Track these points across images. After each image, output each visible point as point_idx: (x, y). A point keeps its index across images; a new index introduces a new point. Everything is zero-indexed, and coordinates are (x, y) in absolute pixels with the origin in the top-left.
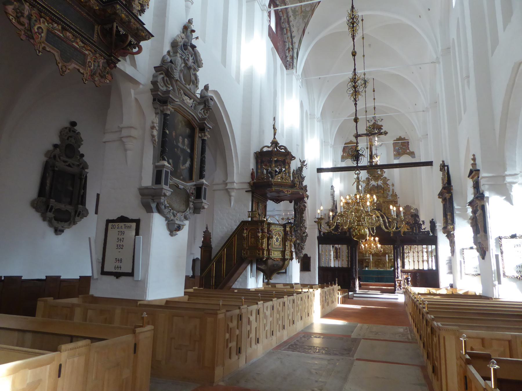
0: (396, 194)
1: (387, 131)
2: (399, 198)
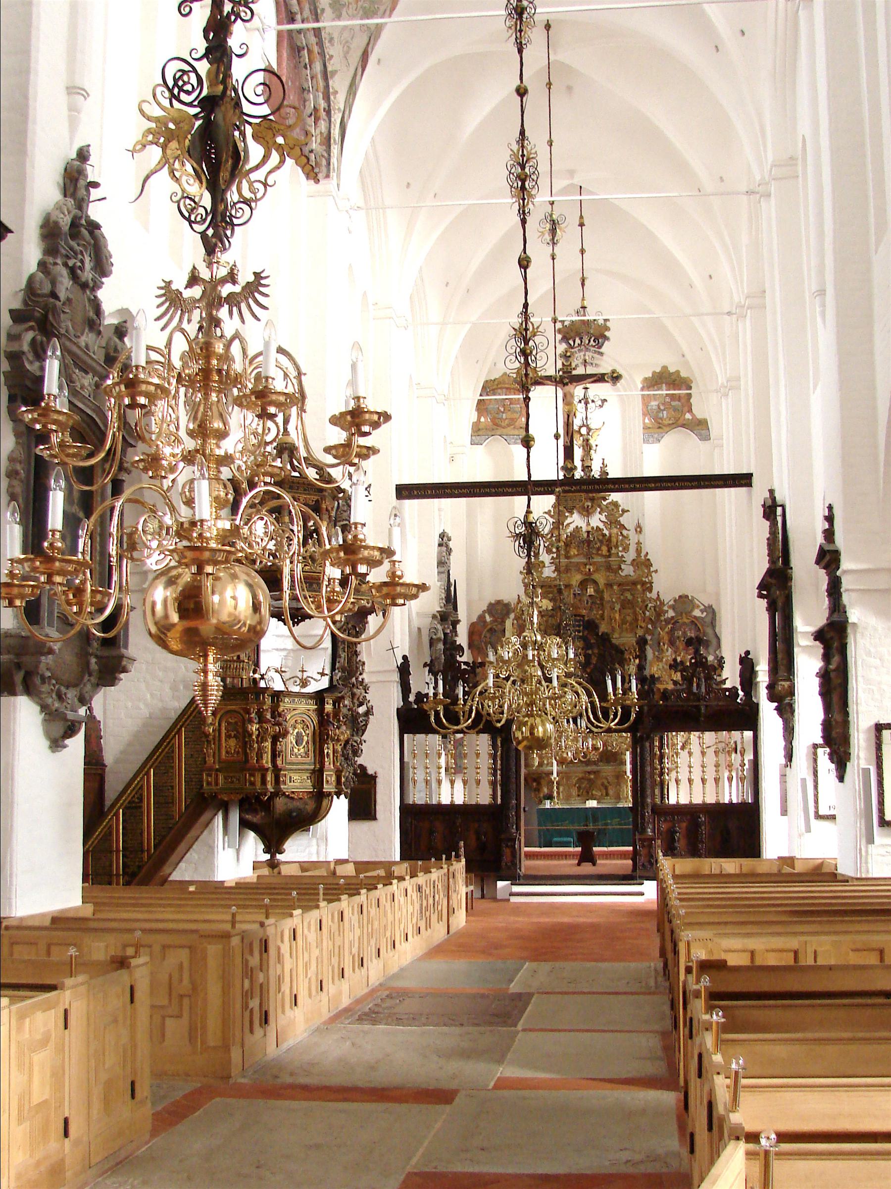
0: (649, 560)
1: (620, 371)
2: (656, 571)
